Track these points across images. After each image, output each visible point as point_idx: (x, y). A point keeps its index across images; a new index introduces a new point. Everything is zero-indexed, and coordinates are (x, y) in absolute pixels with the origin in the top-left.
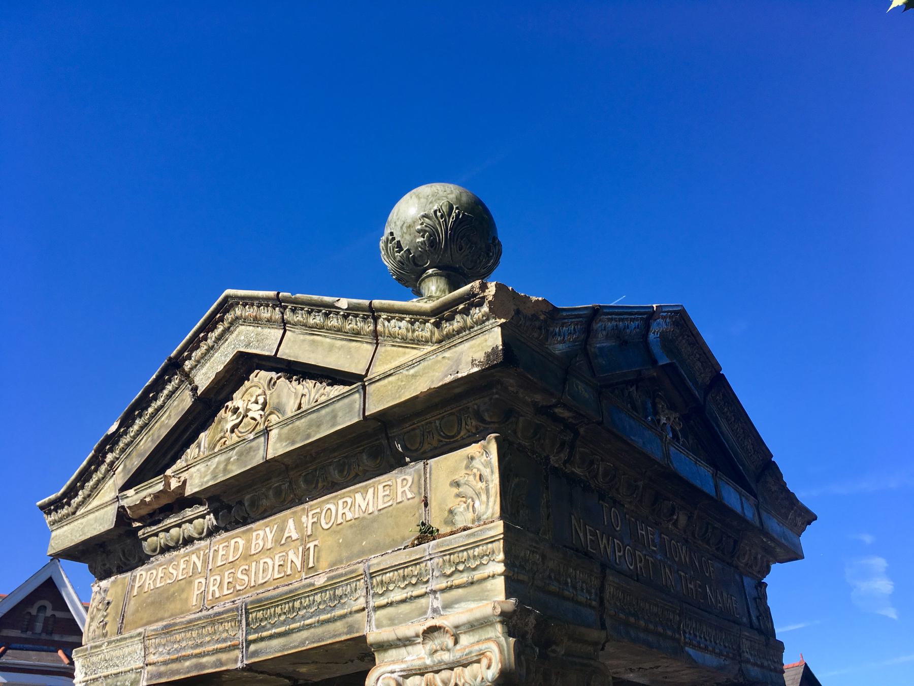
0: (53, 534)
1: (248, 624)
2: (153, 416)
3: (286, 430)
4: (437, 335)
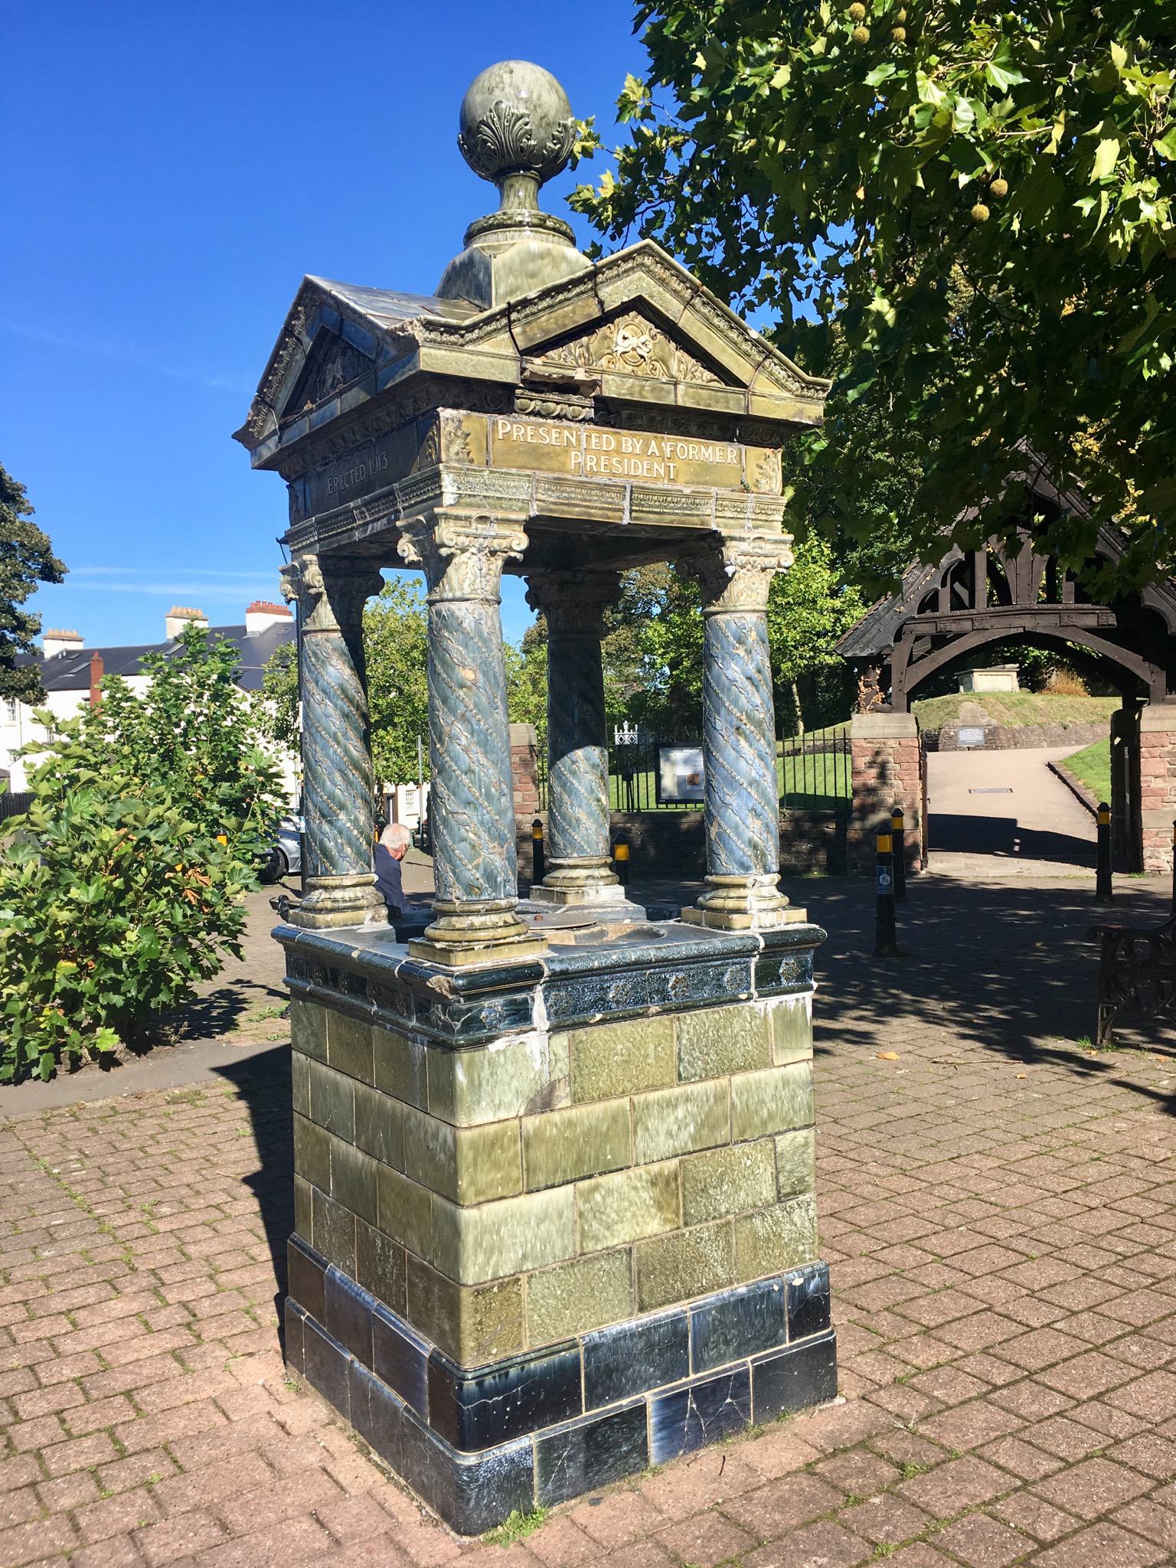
2: (560, 302)
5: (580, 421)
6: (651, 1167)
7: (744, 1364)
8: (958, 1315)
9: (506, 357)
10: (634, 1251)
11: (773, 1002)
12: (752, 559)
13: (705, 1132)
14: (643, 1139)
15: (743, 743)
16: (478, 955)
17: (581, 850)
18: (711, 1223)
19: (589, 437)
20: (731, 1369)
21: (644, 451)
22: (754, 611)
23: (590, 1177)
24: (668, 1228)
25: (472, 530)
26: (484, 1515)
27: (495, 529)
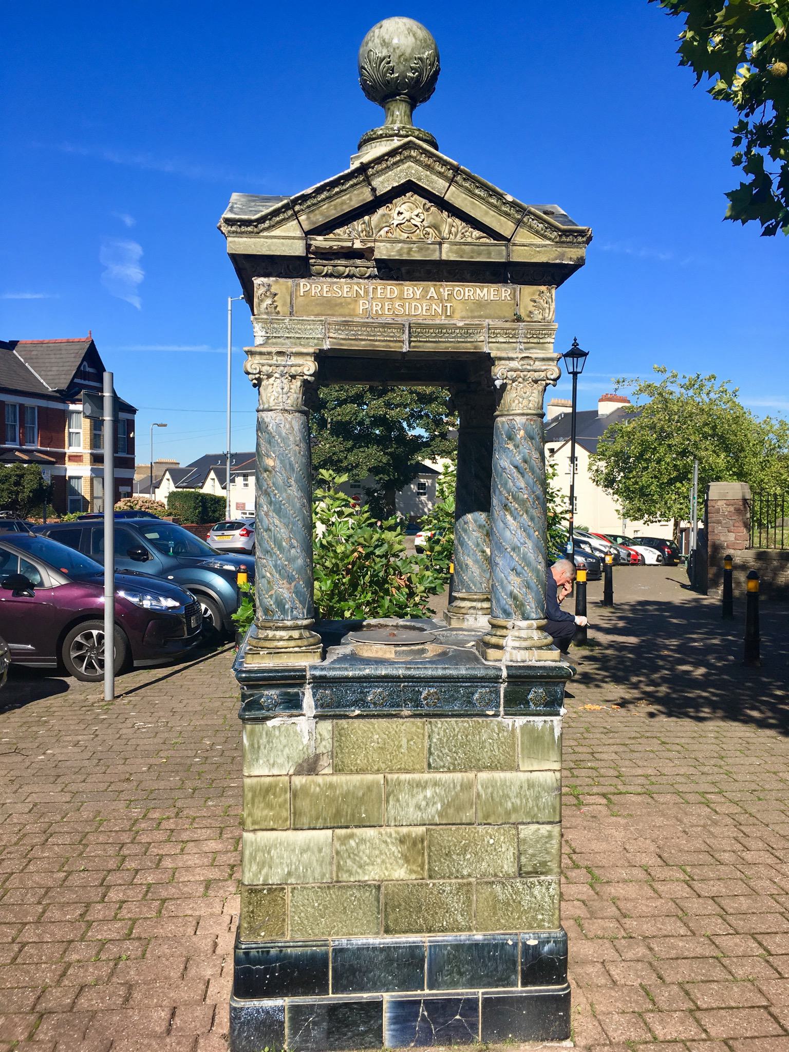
0: (229, 239)
1: (410, 333)
2: (337, 193)
3: (455, 247)
4: (557, 239)
5: (368, 278)
6: (400, 829)
7: (474, 994)
8: (733, 1004)
9: (294, 238)
10: (383, 889)
11: (520, 721)
12: (522, 374)
13: (451, 811)
14: (394, 807)
15: (509, 517)
16: (263, 658)
17: (469, 590)
18: (453, 881)
19: (375, 289)
20: (462, 994)
21: (424, 297)
22: (523, 414)
23: (347, 827)
24: (414, 876)
25: (274, 362)
26: (244, 1043)
27: (294, 360)
